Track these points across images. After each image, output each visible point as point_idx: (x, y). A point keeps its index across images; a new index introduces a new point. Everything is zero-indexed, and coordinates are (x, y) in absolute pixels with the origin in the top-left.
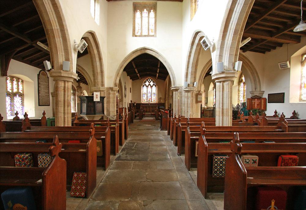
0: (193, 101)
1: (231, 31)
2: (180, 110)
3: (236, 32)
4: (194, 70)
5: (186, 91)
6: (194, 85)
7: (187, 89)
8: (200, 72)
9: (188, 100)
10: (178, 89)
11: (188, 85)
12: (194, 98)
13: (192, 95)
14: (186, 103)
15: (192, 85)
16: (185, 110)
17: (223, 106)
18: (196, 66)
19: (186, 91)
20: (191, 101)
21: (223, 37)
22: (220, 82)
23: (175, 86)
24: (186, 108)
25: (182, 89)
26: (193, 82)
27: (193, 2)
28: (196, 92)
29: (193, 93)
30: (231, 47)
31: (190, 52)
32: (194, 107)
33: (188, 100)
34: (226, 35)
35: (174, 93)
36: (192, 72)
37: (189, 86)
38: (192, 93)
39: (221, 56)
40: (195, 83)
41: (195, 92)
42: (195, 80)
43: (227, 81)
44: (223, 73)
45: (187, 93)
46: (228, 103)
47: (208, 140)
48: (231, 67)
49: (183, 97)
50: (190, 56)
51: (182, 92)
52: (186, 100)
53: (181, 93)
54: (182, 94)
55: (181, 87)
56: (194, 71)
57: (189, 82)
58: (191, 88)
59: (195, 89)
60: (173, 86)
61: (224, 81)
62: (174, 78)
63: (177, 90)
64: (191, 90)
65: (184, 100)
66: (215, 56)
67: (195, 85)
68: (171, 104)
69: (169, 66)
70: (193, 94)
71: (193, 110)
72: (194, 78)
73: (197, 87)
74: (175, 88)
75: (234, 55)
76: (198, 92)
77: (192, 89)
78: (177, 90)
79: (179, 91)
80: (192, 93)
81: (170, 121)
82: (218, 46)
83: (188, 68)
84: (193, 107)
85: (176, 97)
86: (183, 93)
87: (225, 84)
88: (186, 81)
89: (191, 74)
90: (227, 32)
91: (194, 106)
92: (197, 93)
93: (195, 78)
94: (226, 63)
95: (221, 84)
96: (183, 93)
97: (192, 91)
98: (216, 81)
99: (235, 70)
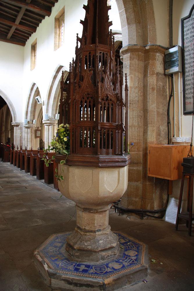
0: (33, 136)
1: (53, 94)
2: (109, 5)
3: (55, 98)
4: (33, 110)
5: (26, 127)
6: (33, 122)
7: (27, 126)
8: (39, 111)
9: (28, 135)
10: (19, 125)
11: (28, 122)
12: (33, 134)
13: (32, 130)
14: (26, 138)
15: (31, 122)
16: (25, 138)
17: (48, 141)
18: (35, 106)
19: (26, 127)
20: (31, 136)
21: (48, 99)
22: (47, 125)
23: (16, 122)
24: (26, 143)
25: (22, 125)
26: (32, 119)
27: (33, 56)
28: (35, 128)
29: (33, 129)
30: (52, 106)
31: (30, 95)
32: (33, 142)
33: (28, 135)
34: (50, 98)
35: (15, 128)
36: (31, 111)
37: (29, 122)
38: (32, 129)
39: (47, 109)
40: (34, 121)
41: (34, 129)
42: (34, 118)
43: (51, 125)
44: (48, 120)
45: (26, 129)
46: (47, 137)
47: (33, 155)
48: (53, 117)
49: (23, 133)
50: (29, 98)
51: (22, 128)
52: (26, 135)
53: (21, 129)
54: (22, 130)
55: (22, 123)
56: (33, 110)
57: (29, 119)
58: (31, 125)
59: (34, 126)
60: (13, 122)
61: (49, 125)
62: (14, 114)
63: (17, 126)
64: (30, 127)
65: (25, 135)
66: (44, 108)
67: (34, 123)
68: (9, 139)
69: (10, 103)
70: (33, 130)
71: (33, 144)
72: (33, 116)
73: (36, 124)
74: (15, 124)
75: (55, 110)
76: (37, 129)
77: (31, 126)
78: (17, 126)
79: (19, 126)
80: (32, 129)
81: (13, 153)
82: (46, 103)
83: (28, 107)
84: (33, 141)
85: (17, 132)
86: (24, 129)
87: (50, 127)
88: (26, 118)
89: (31, 113)
90: (50, 96)
91: (34, 140)
92: (36, 129)
93: (34, 116)
94: (50, 114)
95: (48, 127)
96: (24, 129)
97: (31, 127)
98: (45, 124)
99: (55, 119)
